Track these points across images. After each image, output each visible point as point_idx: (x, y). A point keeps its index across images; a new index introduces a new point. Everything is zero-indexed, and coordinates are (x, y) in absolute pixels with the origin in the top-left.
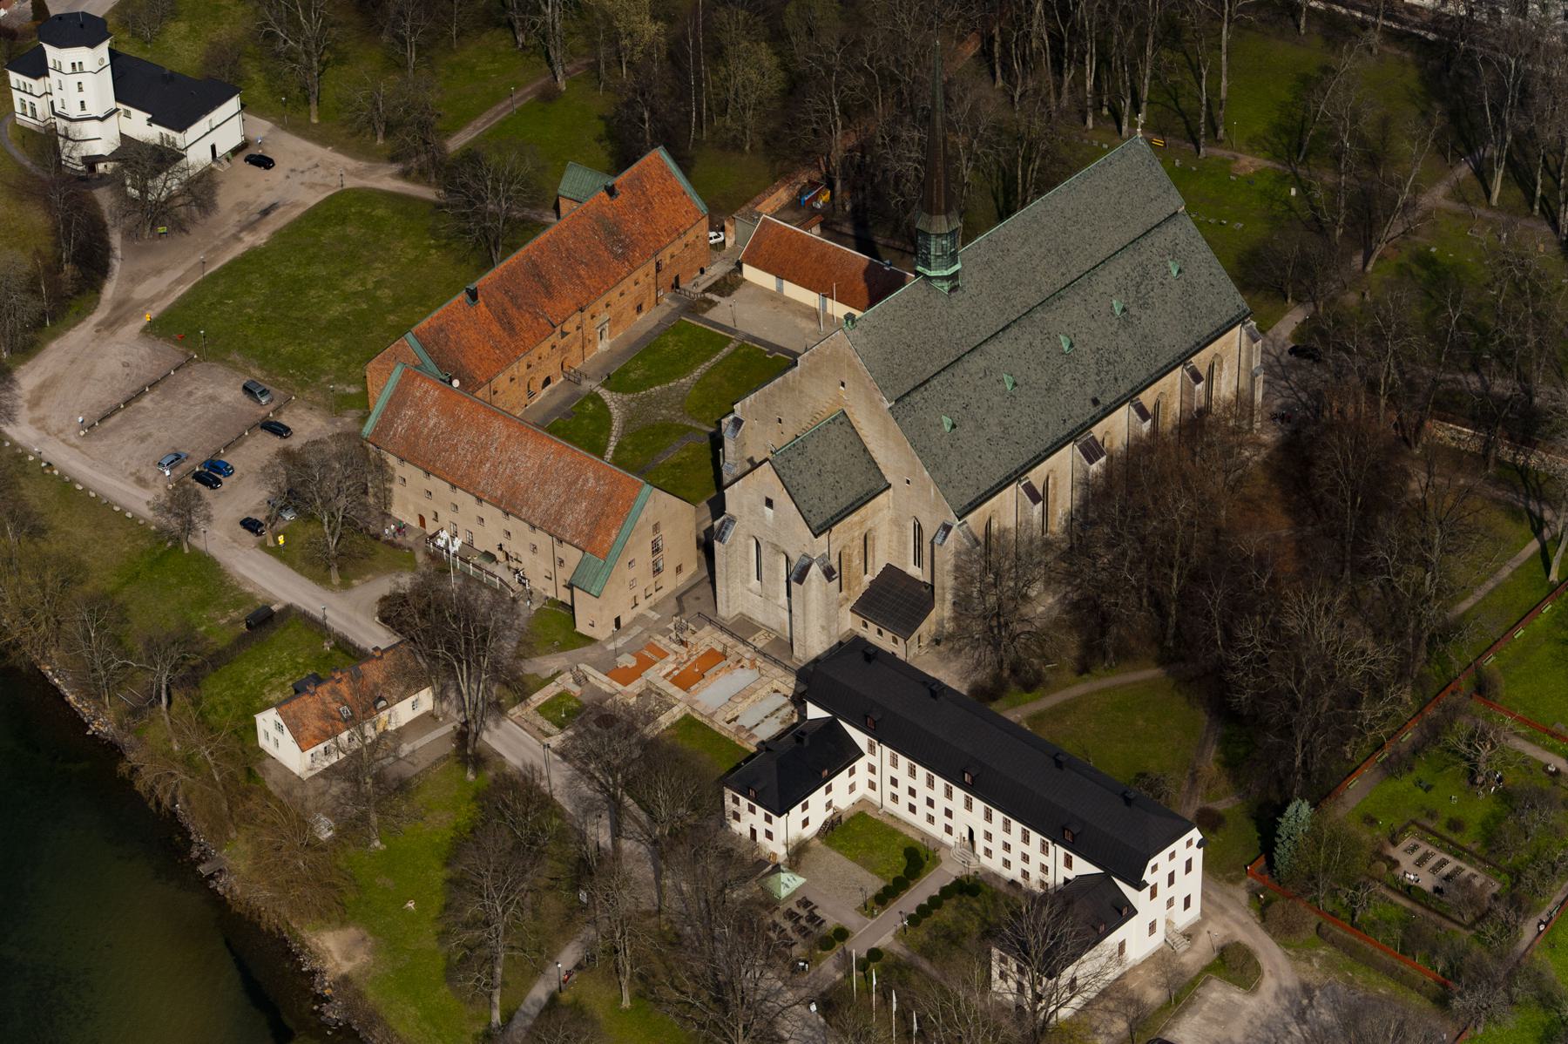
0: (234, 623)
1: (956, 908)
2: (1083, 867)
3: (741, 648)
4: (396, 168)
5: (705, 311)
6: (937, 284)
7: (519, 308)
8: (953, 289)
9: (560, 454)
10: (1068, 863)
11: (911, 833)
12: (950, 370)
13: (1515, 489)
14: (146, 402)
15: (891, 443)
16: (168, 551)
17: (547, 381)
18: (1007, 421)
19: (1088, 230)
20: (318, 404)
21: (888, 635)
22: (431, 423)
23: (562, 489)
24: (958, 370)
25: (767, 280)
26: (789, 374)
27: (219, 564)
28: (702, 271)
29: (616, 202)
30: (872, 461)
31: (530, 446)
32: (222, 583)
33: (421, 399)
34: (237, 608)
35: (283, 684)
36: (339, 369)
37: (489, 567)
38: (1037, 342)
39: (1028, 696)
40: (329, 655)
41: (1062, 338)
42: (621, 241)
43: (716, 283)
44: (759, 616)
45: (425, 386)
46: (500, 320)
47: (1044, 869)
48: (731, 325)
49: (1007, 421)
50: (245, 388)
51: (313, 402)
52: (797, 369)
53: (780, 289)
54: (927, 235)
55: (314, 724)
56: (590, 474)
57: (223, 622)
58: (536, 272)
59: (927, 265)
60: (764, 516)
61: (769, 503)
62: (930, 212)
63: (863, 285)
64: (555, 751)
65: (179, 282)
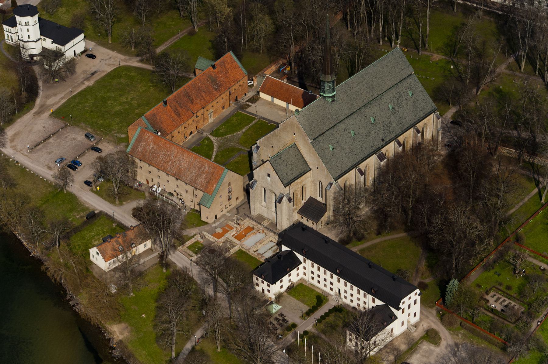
0: (82, 217)
1: (334, 317)
2: (378, 302)
3: (259, 226)
4: (138, 58)
5: (246, 108)
6: (327, 99)
7: (182, 107)
8: (333, 101)
9: (196, 158)
10: (373, 301)
11: (318, 290)
12: (332, 129)
13: (530, 171)
14: (51, 140)
15: (311, 155)
16: (59, 192)
17: (191, 133)
18: (352, 147)
19: (380, 80)
20: (111, 141)
21: (310, 221)
22: (151, 148)
23: (196, 170)
24: (335, 129)
25: (268, 98)
26: (276, 130)
27: (76, 197)
28: (245, 95)
29: (215, 70)
30: (305, 161)
31: (185, 156)
32: (78, 203)
33: (147, 139)
34: (83, 212)
35: (99, 238)
36: (118, 129)
37: (171, 198)
38: (362, 119)
39: (359, 243)
40: (115, 229)
41: (371, 118)
42: (217, 84)
43: (250, 99)
44: (265, 215)
45: (149, 134)
46: (175, 112)
47: (365, 303)
48: (256, 113)
49: (352, 147)
50: (86, 135)
51: (109, 140)
52: (278, 129)
53: (273, 101)
54: (324, 82)
55: (110, 253)
56: (206, 165)
57: (78, 217)
58: (187, 95)
59: (324, 92)
60: (267, 180)
61: (269, 175)
62: (325, 74)
63: (302, 99)
64: (194, 262)
65: (63, 98)
